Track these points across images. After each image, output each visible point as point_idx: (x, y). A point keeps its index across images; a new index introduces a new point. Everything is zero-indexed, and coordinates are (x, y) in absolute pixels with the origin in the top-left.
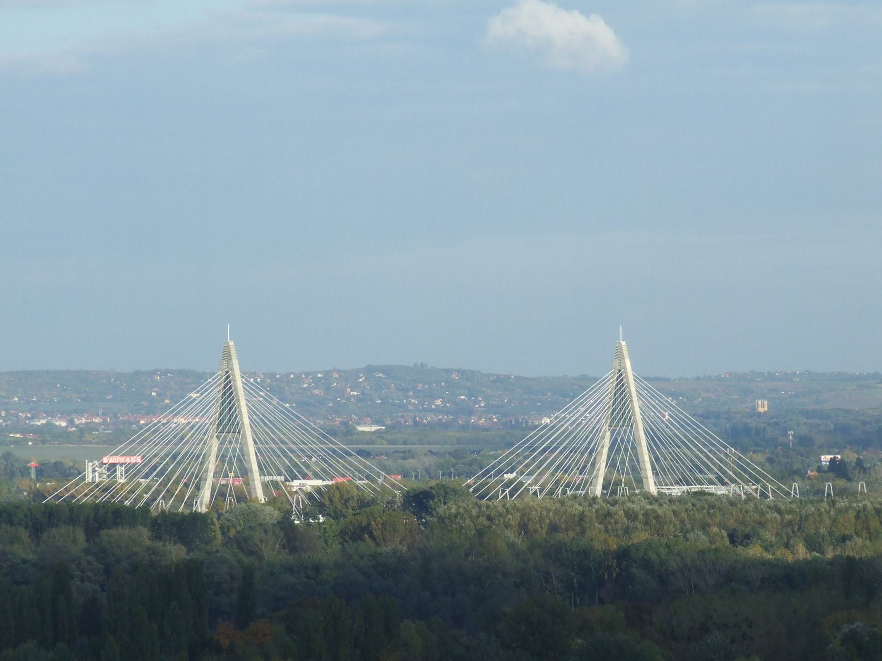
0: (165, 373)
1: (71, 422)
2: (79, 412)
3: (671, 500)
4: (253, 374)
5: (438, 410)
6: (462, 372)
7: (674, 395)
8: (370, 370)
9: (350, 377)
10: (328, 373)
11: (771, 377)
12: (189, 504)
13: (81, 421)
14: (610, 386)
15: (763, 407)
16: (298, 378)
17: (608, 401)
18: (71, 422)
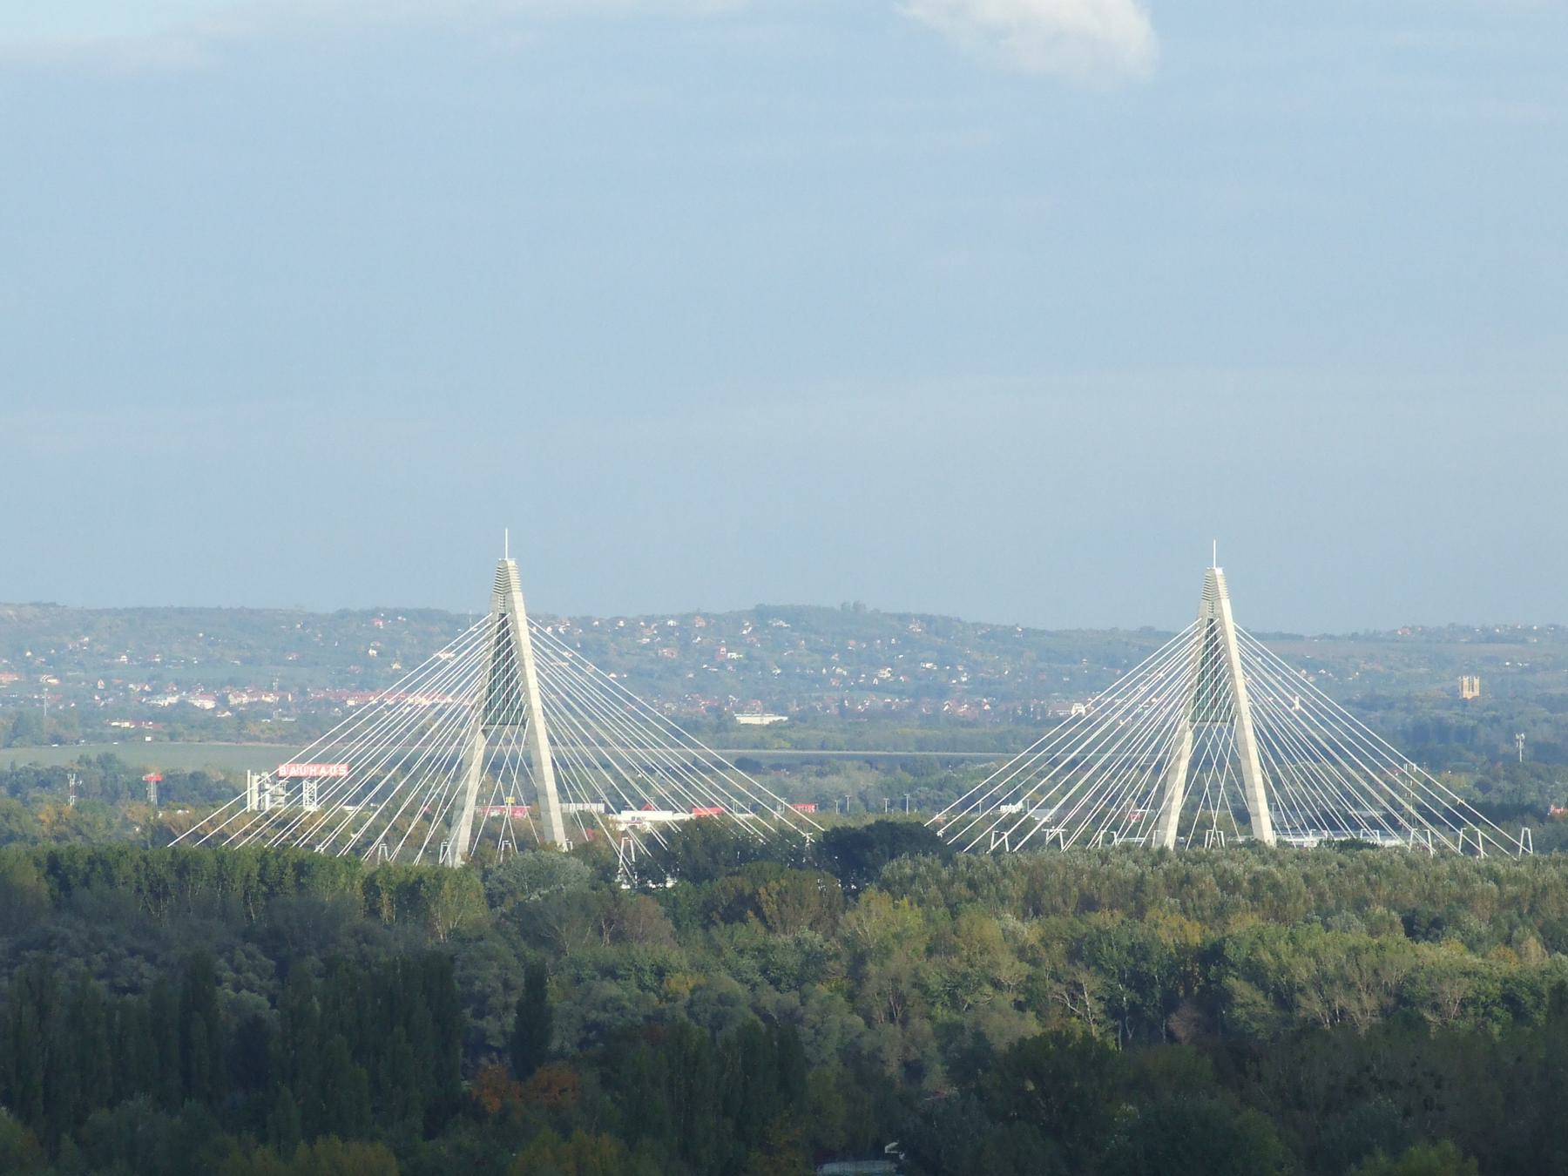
0: (391, 614)
1: (222, 701)
2: (236, 683)
3: (1301, 856)
4: (551, 619)
5: (884, 688)
6: (927, 620)
7: (1311, 666)
8: (762, 615)
10: (685, 619)
12: (432, 853)
14: (1195, 648)
15: (1471, 689)
16: (633, 629)
18: (222, 701)
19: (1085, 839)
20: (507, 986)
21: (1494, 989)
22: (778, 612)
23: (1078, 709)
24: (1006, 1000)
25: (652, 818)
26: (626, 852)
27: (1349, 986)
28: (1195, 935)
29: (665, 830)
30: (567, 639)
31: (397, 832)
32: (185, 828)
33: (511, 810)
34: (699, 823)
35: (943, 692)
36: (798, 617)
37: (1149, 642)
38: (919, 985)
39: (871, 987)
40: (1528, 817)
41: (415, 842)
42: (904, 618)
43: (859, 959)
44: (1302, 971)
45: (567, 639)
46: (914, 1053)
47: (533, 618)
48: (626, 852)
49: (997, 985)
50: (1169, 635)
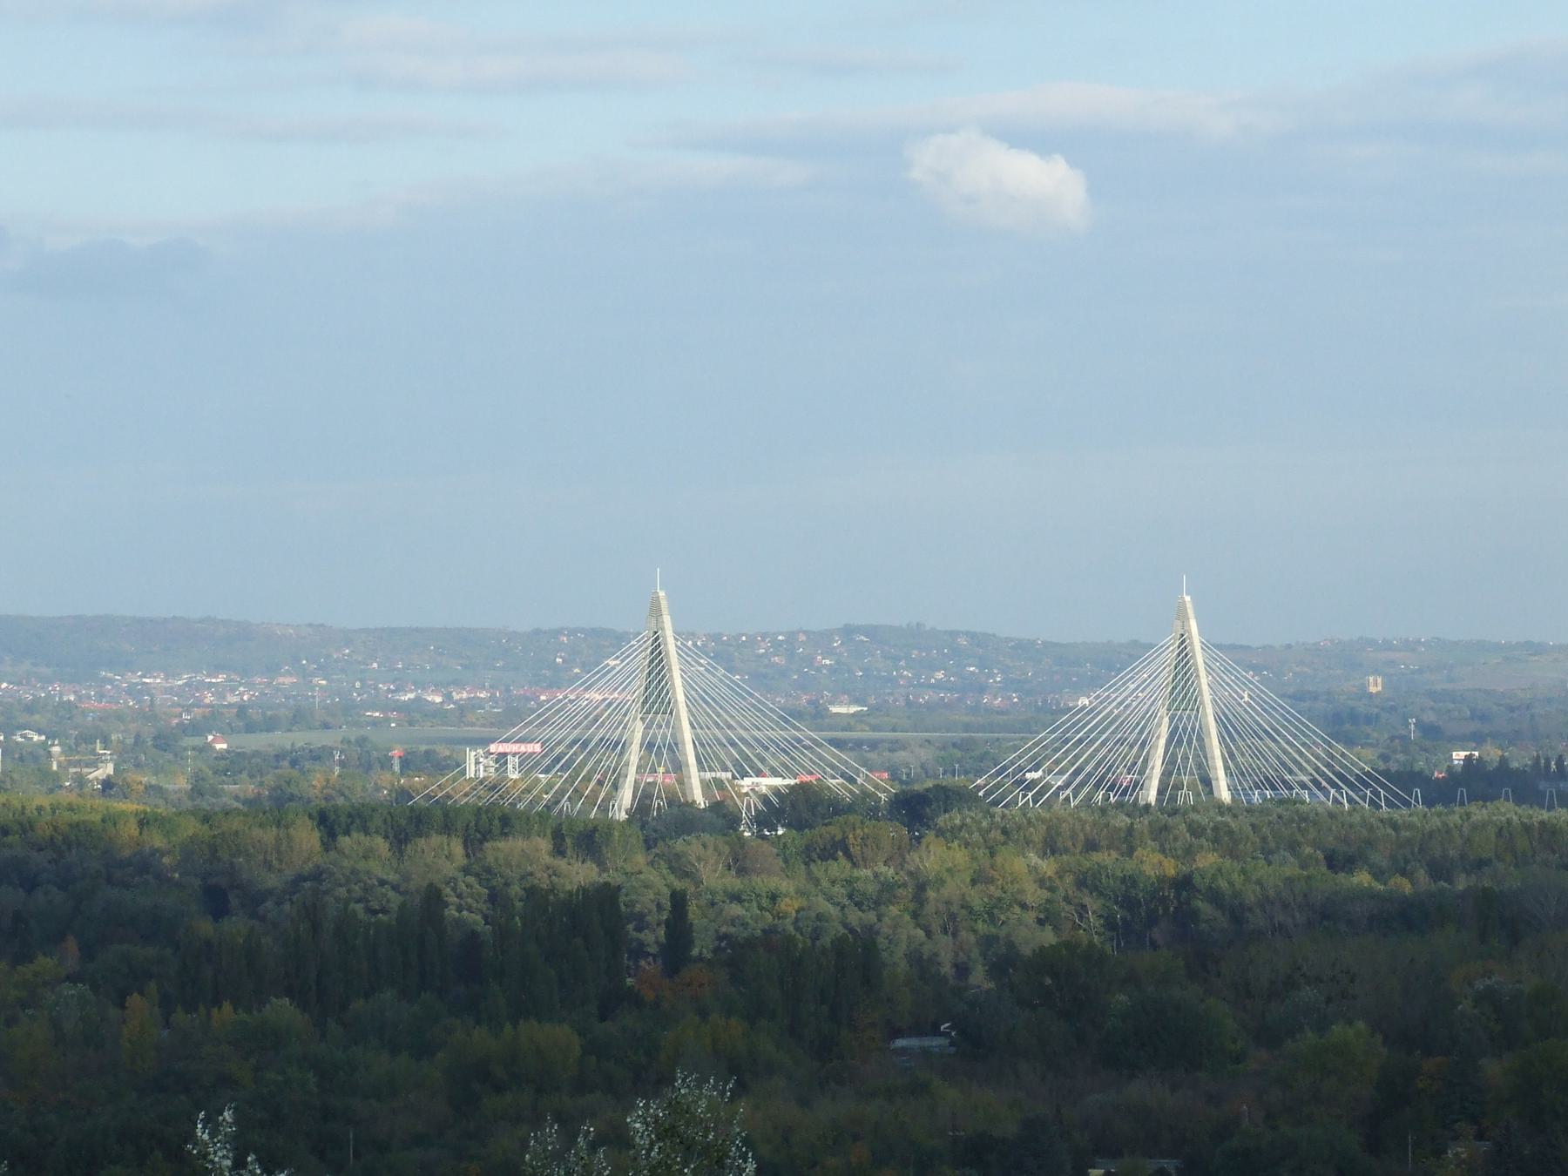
1: (448, 697)
2: (459, 684)
5: (939, 686)
7: (1256, 669)
8: (848, 632)
9: (820, 640)
10: (791, 636)
11: (1387, 646)
12: (604, 809)
13: (461, 695)
14: (1170, 655)
15: (1375, 685)
16: (752, 641)
17: (1166, 676)
19: (1089, 797)
28: (1171, 868)
34: (803, 787)
37: (1135, 652)
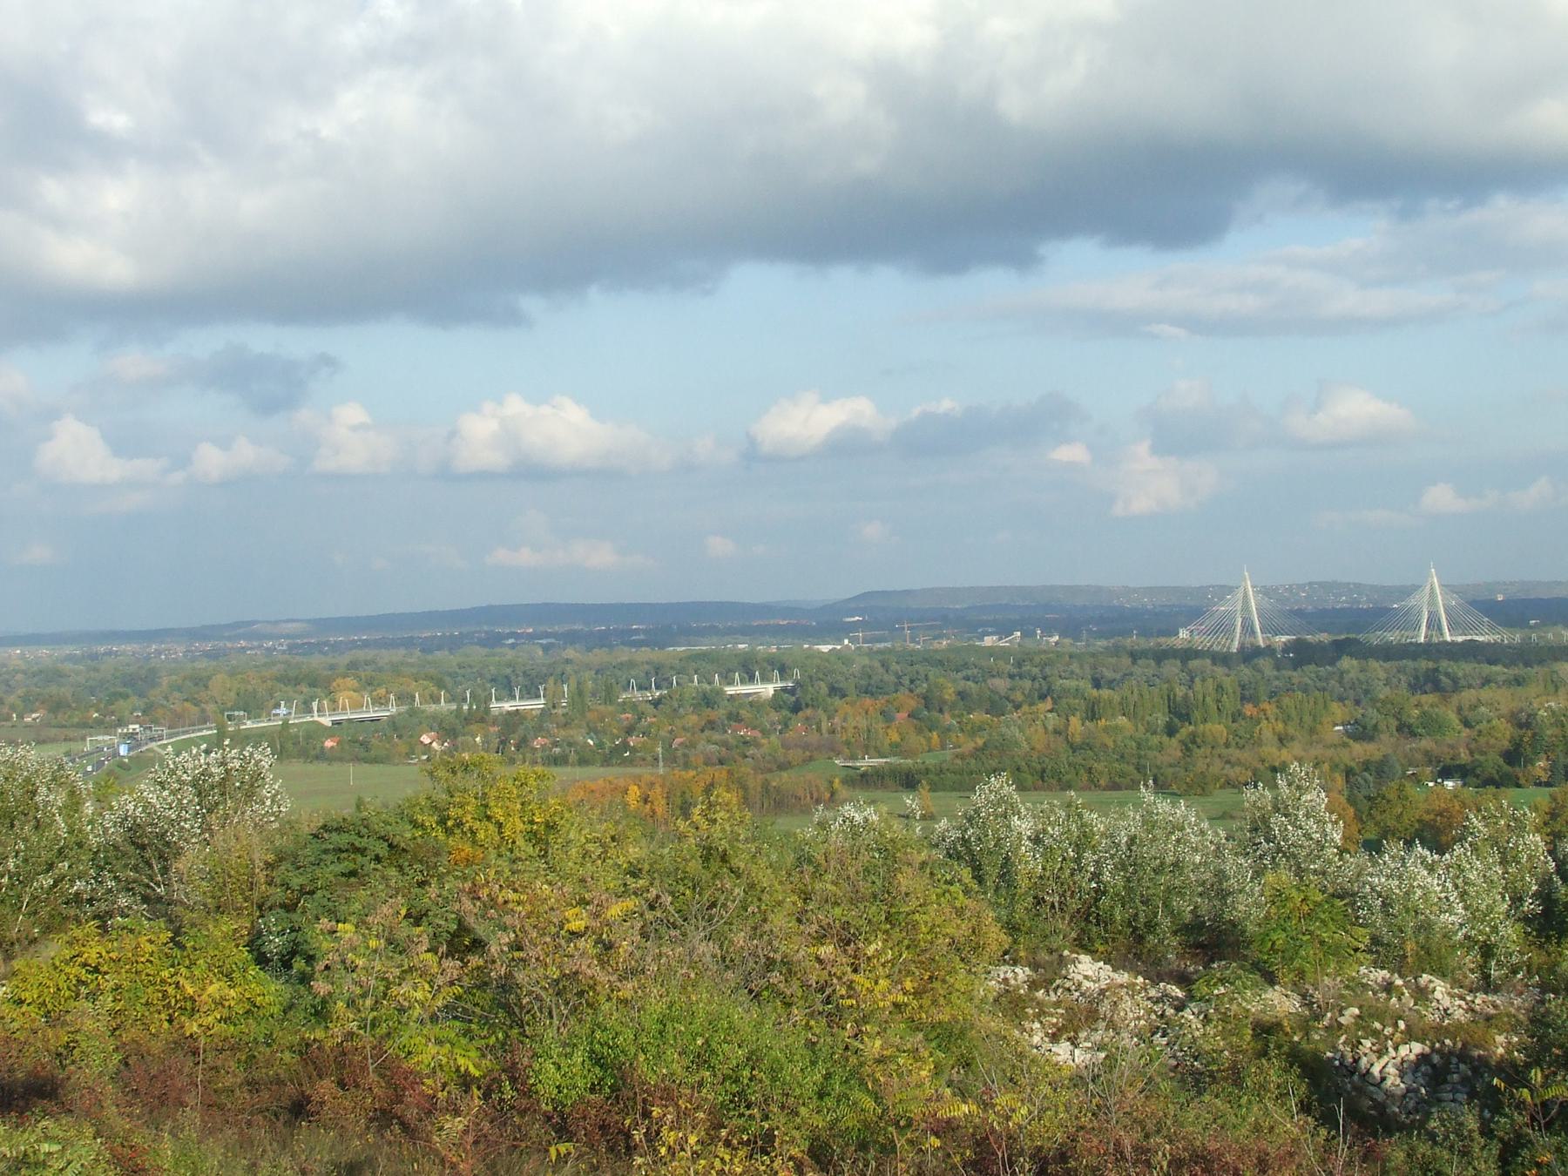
0: (1213, 587)
6: (1354, 584)
12: (1229, 648)
14: (1428, 587)
16: (1277, 588)
20: (1250, 683)
21: (1512, 678)
22: (1316, 583)
23: (1395, 606)
24: (1381, 683)
25: (1284, 639)
26: (1279, 647)
27: (1473, 678)
29: (1289, 641)
30: (1260, 592)
31: (1219, 643)
32: (647, 685)
33: (1248, 640)
35: (1359, 602)
36: (1322, 585)
38: (1358, 679)
39: (1346, 681)
40: (741, 793)
41: (1224, 646)
42: (1349, 584)
43: (1342, 673)
44: (1460, 674)
45: (1260, 592)
46: (1357, 698)
47: (1253, 587)
48: (1279, 647)
49: (1378, 679)
50: (1420, 587)
